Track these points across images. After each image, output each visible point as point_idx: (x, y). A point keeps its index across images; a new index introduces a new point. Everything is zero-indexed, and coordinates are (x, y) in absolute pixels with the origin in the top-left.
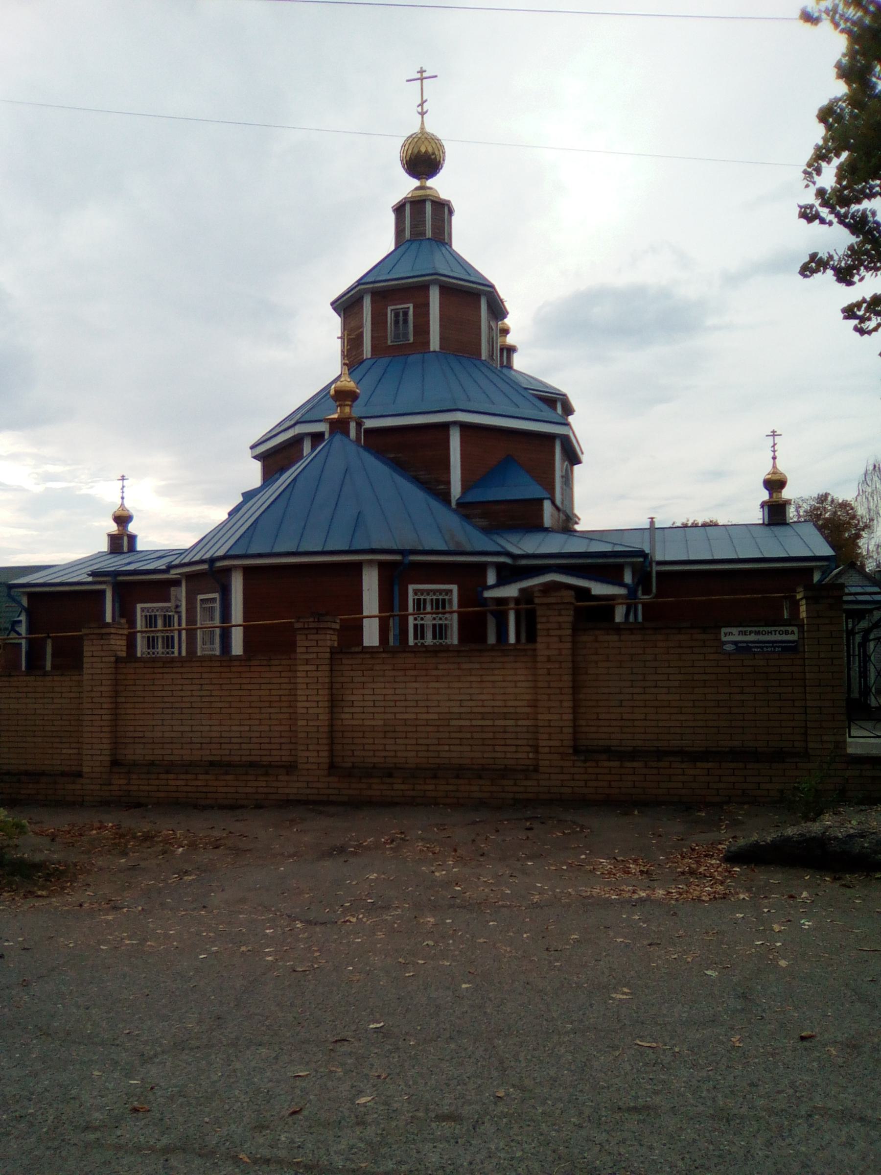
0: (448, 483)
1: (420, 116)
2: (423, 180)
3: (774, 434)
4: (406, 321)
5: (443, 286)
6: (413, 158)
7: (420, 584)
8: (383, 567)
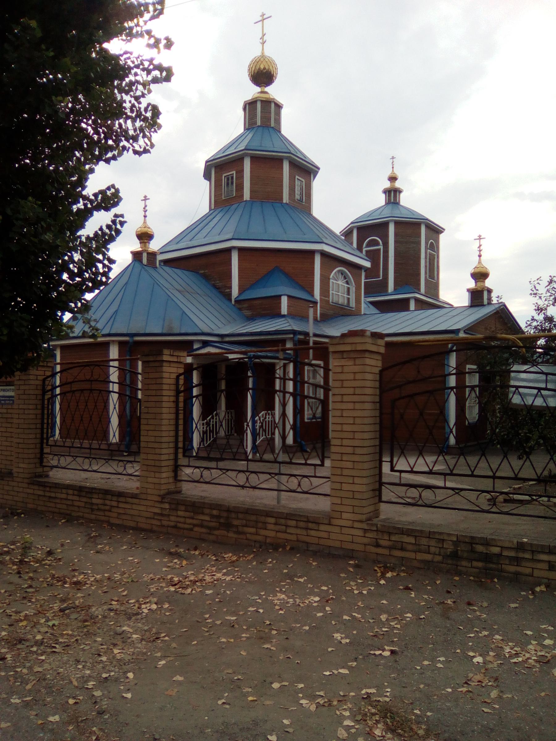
0: (230, 288)
1: (261, 45)
2: (263, 87)
3: (480, 238)
4: (232, 183)
5: (254, 157)
8: (121, 344)
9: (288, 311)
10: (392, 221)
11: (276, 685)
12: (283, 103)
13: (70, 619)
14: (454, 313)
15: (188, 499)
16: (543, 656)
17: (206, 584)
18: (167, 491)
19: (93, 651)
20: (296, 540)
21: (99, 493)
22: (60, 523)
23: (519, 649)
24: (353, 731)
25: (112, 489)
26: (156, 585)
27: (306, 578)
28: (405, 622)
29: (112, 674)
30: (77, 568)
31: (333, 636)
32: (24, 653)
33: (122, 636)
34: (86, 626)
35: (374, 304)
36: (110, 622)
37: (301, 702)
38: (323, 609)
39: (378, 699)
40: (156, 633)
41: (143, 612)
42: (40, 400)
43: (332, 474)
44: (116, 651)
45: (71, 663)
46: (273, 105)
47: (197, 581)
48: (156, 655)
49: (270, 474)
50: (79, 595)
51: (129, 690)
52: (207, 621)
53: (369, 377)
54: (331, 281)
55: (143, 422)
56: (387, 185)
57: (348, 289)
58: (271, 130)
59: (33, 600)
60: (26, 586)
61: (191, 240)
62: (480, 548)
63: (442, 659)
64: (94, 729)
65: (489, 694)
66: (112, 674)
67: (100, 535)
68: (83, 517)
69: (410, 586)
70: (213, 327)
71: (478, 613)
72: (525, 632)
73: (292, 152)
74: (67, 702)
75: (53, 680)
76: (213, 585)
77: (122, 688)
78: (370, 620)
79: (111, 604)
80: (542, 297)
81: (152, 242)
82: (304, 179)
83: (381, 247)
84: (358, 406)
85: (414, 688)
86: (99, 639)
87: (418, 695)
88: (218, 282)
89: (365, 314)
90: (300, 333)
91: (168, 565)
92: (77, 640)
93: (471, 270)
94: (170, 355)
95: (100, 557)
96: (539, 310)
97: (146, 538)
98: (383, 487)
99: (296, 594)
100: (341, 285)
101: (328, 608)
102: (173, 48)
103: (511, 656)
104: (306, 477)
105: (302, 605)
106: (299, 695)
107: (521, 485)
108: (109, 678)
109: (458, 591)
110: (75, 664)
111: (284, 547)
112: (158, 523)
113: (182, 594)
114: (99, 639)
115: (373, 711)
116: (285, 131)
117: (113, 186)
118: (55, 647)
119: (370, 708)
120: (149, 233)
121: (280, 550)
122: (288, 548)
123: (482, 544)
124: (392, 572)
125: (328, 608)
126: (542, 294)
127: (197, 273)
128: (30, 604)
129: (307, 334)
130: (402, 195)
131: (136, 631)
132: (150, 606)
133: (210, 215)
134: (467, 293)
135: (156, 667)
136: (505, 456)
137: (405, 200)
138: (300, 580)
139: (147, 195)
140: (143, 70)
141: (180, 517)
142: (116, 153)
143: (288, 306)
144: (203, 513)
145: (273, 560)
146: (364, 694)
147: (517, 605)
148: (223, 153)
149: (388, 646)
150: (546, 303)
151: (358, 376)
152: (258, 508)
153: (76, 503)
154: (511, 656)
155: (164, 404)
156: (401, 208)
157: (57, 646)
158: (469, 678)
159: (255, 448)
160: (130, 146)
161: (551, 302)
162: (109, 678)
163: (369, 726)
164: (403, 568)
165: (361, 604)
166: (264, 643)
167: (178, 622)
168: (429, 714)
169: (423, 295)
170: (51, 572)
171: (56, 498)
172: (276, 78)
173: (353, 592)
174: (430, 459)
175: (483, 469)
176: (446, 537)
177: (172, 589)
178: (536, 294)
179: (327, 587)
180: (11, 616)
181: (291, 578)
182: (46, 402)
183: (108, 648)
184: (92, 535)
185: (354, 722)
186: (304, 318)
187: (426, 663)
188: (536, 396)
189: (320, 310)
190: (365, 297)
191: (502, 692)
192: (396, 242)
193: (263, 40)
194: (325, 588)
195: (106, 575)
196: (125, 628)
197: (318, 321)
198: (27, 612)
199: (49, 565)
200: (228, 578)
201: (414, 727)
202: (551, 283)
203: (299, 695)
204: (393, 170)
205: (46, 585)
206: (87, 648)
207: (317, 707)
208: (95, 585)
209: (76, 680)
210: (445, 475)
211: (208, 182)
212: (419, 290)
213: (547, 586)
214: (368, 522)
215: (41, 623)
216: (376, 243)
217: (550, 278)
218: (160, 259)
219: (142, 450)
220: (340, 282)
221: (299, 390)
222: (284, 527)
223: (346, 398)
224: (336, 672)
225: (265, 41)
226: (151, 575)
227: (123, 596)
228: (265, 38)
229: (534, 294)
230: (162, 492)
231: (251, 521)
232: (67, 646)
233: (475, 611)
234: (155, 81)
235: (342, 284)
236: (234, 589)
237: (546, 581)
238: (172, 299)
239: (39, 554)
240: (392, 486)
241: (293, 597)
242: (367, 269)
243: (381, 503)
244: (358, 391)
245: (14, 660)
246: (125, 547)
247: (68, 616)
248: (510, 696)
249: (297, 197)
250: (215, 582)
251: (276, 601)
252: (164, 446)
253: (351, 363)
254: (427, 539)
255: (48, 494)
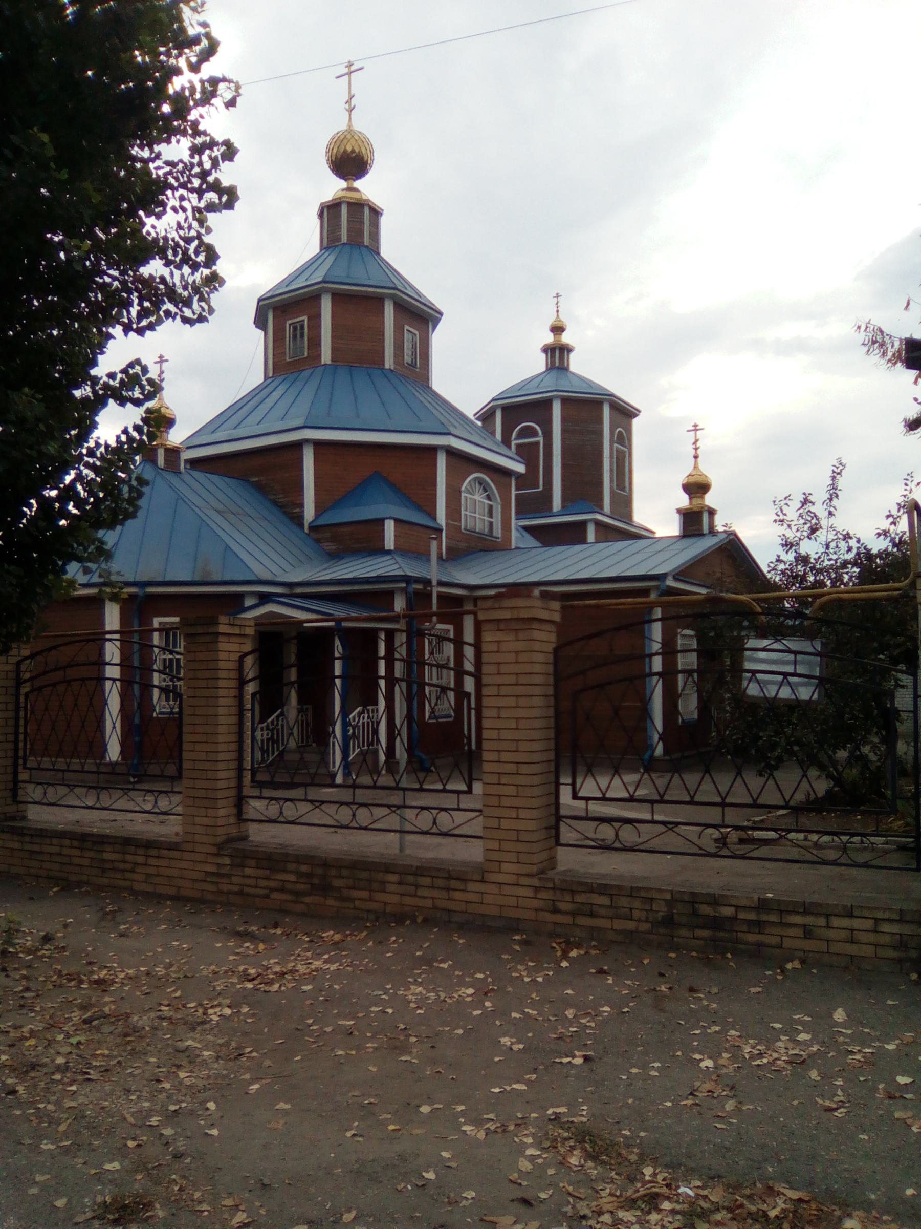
0: (301, 506)
1: (347, 113)
3: (696, 428)
4: (302, 335)
6: (339, 157)
7: (164, 616)
9: (395, 544)
10: (557, 397)
11: (425, 1109)
12: (383, 208)
13: (102, 1033)
14: (658, 547)
15: (261, 849)
16: (795, 1054)
17: (300, 976)
18: (226, 837)
19: (147, 1075)
20: (431, 906)
21: (115, 843)
22: (51, 893)
23: (764, 1047)
24: (540, 1161)
25: (136, 837)
26: (223, 981)
27: (450, 963)
28: (601, 1018)
29: (184, 1105)
30: (95, 961)
31: (500, 1041)
32: (43, 1083)
33: (187, 1054)
34: (129, 1042)
35: (530, 530)
36: (165, 1035)
37: (464, 1128)
38: (480, 1005)
39: (571, 1119)
40: (236, 1049)
41: (212, 1020)
42: (12, 695)
43: (484, 805)
44: (182, 1075)
45: (118, 1093)
46: (367, 211)
47: (286, 973)
48: (242, 1077)
49: (389, 806)
50: (107, 999)
51: (212, 1125)
52: (311, 1028)
53: (540, 657)
54: (463, 495)
55: (186, 729)
56: (549, 338)
57: (491, 507)
58: (364, 250)
59: (37, 1009)
60: (21, 988)
61: (235, 428)
62: (705, 910)
63: (657, 1065)
64: (174, 1177)
65: (723, 1107)
66: (184, 1105)
67: (120, 910)
68: (87, 883)
69: (606, 968)
70: (274, 569)
71: (705, 1002)
72: (771, 1025)
73: (399, 288)
74: (126, 1145)
75: (96, 1117)
76: (311, 977)
77: (202, 1122)
78: (551, 1018)
79: (160, 1011)
80: (792, 526)
81: (172, 431)
82: (417, 330)
83: (540, 439)
84: (522, 702)
85: (620, 1104)
86: (153, 1060)
87: (626, 1112)
88: (281, 496)
89: (517, 548)
90: (417, 580)
91: (237, 951)
92: (119, 1062)
93: (681, 478)
94: (230, 624)
95: (127, 943)
96: (788, 545)
97: (195, 913)
98: (561, 823)
99: (439, 987)
100: (479, 501)
101: (488, 1004)
102: (237, 158)
103: (753, 1058)
104: (445, 810)
105: (449, 1000)
106: (460, 1120)
107: (765, 817)
108: (180, 1111)
109: (675, 973)
110: (124, 1094)
111: (414, 920)
112: (213, 888)
113: (265, 991)
114: (153, 1060)
115: (566, 1135)
116: (386, 252)
117: (138, 362)
118: (88, 1073)
119: (560, 1131)
120: (167, 415)
121: (408, 922)
122: (420, 919)
123: (708, 904)
124: (577, 949)
125: (488, 1004)
126: (792, 521)
127: (248, 481)
128: (33, 1015)
129: (427, 582)
130: (572, 355)
131: (205, 1046)
132: (221, 1011)
133: (265, 387)
134: (678, 516)
135: (247, 1093)
136: (739, 773)
137: (576, 363)
138: (442, 965)
139: (164, 354)
140: (192, 190)
141: (249, 877)
142: (153, 319)
143: (395, 536)
144: (285, 871)
145: (398, 938)
146: (551, 1115)
147: (760, 990)
148: (287, 286)
149: (579, 1051)
150: (798, 534)
151: (523, 657)
152: (372, 860)
153: (76, 861)
154: (753, 1058)
155: (222, 701)
156: (569, 375)
157: (92, 1072)
158: (695, 1088)
159: (347, 766)
160: (177, 311)
161: (805, 534)
162: (180, 1111)
163: (561, 1154)
164: (593, 943)
165: (537, 996)
166: (401, 1055)
167: (268, 1031)
168: (642, 1134)
169: (607, 516)
170: (54, 966)
171: (41, 853)
172: (371, 167)
173: (523, 980)
174: (631, 778)
175: (707, 792)
176: (655, 895)
177: (250, 985)
178: (782, 521)
179: (484, 973)
180: (8, 1032)
181: (429, 963)
182: (22, 699)
183: (169, 1072)
184: (108, 910)
185: (540, 1151)
186: (422, 555)
187: (634, 1071)
188: (781, 684)
189: (446, 542)
190: (517, 519)
191: (740, 1103)
192: (563, 431)
193: (350, 105)
194: (480, 976)
195: (142, 969)
196: (189, 1043)
197: (444, 560)
198: (32, 1027)
199: (49, 957)
200: (333, 967)
201: (623, 1152)
202: (806, 504)
203: (460, 1120)
204: (558, 316)
205: (51, 987)
206: (137, 1072)
207: (487, 1135)
208: (128, 985)
209: (132, 1116)
210: (652, 802)
211: (263, 333)
212: (602, 507)
213: (803, 962)
214: (542, 876)
215: (59, 1041)
216: (531, 432)
217: (804, 496)
218: (186, 458)
219: (185, 774)
220: (477, 497)
221: (415, 672)
222: (413, 888)
223: (504, 691)
224: (508, 1088)
225: (354, 108)
226: (213, 967)
227: (176, 998)
228: (353, 102)
229: (780, 521)
230: (219, 840)
231: (361, 879)
232: (107, 1070)
233: (700, 999)
234: (211, 208)
235: (482, 500)
236: (345, 982)
237: (801, 954)
238: (208, 525)
239: (27, 940)
240: (577, 822)
241: (433, 990)
242: (519, 476)
243: (559, 848)
244: (523, 679)
245: (30, 1094)
246: (164, 927)
247: (98, 1029)
248: (751, 1107)
249: (407, 359)
250: (315, 973)
251: (410, 997)
252: (221, 766)
253: (511, 636)
254: (629, 899)
255: (28, 847)
